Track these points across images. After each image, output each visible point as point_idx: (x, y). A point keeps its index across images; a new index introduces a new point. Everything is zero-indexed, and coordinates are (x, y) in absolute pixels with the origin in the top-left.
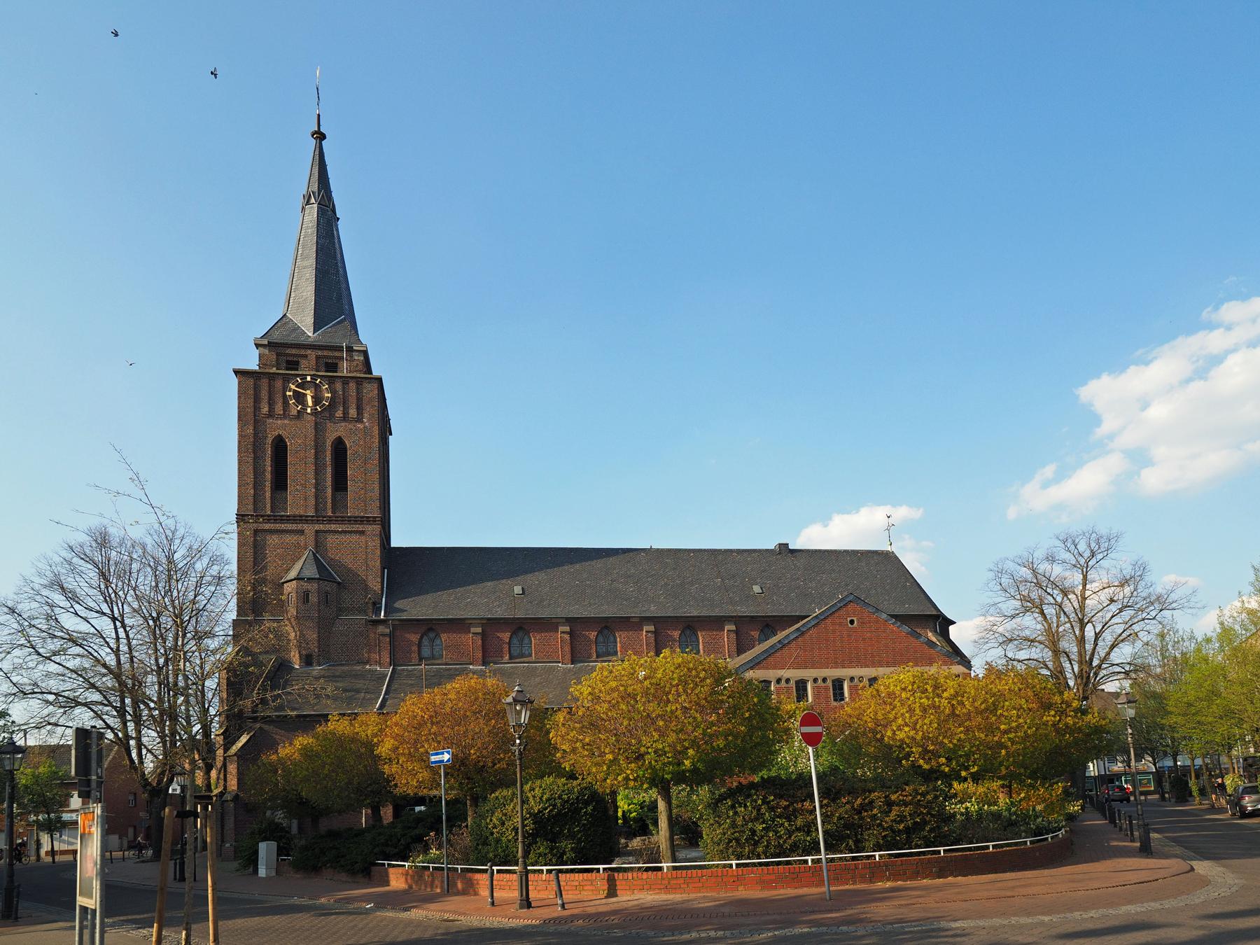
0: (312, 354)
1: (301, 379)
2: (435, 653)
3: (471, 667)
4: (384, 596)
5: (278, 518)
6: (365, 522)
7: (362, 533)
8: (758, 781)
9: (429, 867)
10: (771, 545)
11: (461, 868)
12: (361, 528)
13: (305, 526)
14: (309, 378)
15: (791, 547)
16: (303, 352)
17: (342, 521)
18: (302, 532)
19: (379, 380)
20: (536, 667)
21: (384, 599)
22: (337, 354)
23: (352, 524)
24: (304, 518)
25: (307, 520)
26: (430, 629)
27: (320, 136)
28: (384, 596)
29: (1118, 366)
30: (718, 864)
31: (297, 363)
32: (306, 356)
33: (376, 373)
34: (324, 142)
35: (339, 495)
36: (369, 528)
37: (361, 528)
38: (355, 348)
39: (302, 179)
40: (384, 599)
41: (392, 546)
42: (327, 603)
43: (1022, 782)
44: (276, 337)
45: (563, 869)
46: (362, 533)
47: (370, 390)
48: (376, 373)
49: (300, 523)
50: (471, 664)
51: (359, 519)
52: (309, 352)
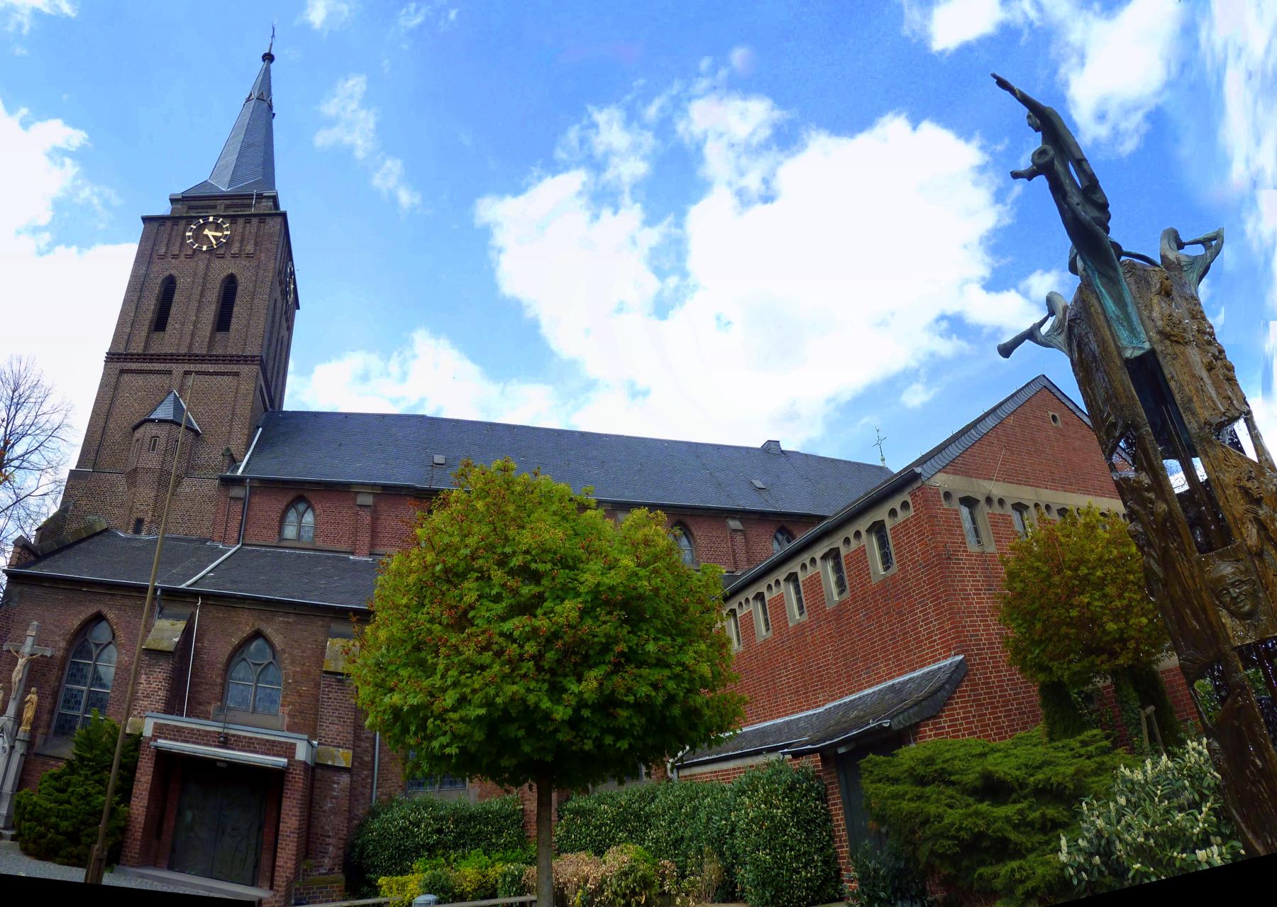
2: (302, 533)
3: (351, 557)
4: (249, 453)
7: (237, 374)
8: (499, 716)
10: (758, 443)
12: (234, 368)
13: (174, 366)
14: (211, 219)
15: (784, 447)
16: (212, 203)
17: (216, 360)
18: (169, 372)
19: (284, 215)
21: (247, 456)
22: (249, 201)
25: (177, 360)
26: (301, 499)
27: (269, 58)
28: (249, 453)
29: (1227, 163)
33: (282, 209)
34: (273, 65)
35: (219, 335)
36: (245, 369)
39: (246, 85)
40: (247, 456)
41: (285, 408)
43: (373, 692)
46: (237, 374)
47: (273, 225)
48: (282, 209)
50: (352, 553)
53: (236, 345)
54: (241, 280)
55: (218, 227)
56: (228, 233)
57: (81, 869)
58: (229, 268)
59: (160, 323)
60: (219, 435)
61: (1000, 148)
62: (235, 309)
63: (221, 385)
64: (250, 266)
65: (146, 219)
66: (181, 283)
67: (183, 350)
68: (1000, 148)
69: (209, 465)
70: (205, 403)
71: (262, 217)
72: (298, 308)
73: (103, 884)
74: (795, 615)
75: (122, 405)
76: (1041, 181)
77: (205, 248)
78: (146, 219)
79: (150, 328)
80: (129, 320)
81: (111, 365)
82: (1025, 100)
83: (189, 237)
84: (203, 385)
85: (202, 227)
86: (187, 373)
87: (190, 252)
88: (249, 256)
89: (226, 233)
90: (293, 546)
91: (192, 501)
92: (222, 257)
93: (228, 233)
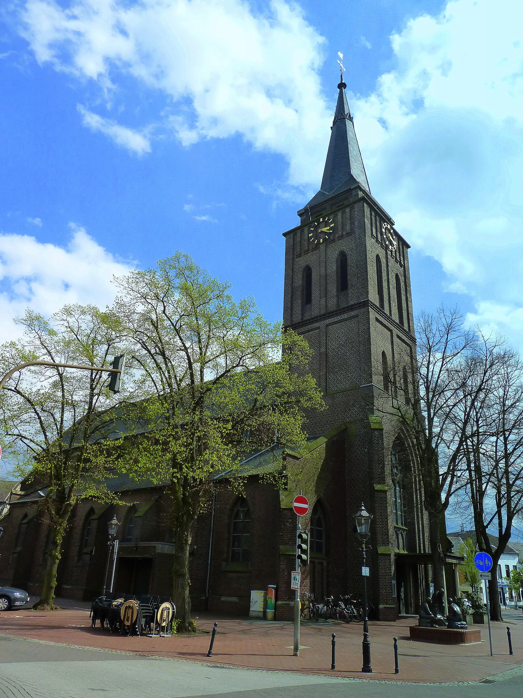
25: (307, 323)
54: (348, 253)
55: (326, 224)
56: (333, 225)
57: (473, 524)
59: (308, 299)
61: (274, 205)
65: (285, 235)
67: (323, 312)
68: (274, 205)
72: (408, 247)
73: (474, 529)
74: (480, 434)
77: (321, 241)
78: (285, 235)
79: (302, 302)
83: (311, 237)
85: (316, 228)
86: (327, 325)
87: (314, 246)
89: (331, 226)
92: (334, 241)
93: (333, 225)
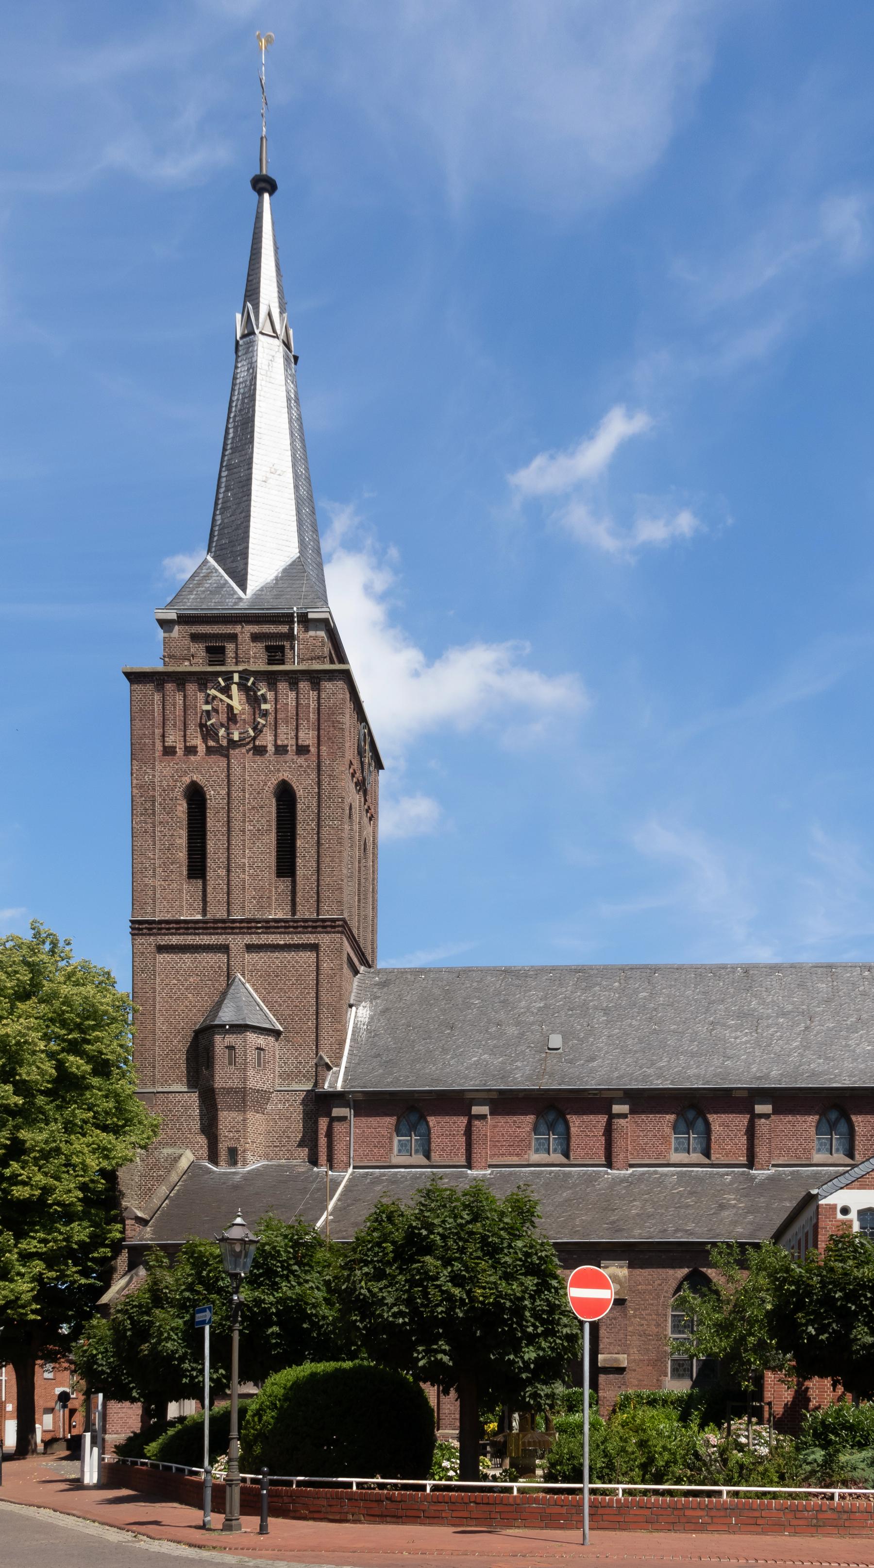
0: (245, 632)
1: (224, 680)
3: (469, 1172)
5: (318, 924)
6: (145, 931)
9: (158, 1465)
11: (163, 1466)
12: (311, 939)
20: (570, 1172)
23: (300, 933)
24: (328, 923)
25: (233, 928)
30: (676, 1483)
31: (222, 650)
32: (233, 638)
37: (311, 939)
38: (311, 616)
42: (259, 1065)
44: (191, 604)
45: (659, 1490)
46: (315, 947)
49: (221, 934)
51: (310, 924)
52: (238, 629)
53: (308, 901)
58: (279, 770)
60: (305, 1032)
62: (299, 843)
63: (297, 962)
64: (308, 766)
66: (215, 797)
69: (300, 1072)
70: (281, 989)
71: (315, 678)
72: (379, 766)
75: (171, 997)
76: (202, 1524)
80: (394, 1520)
81: (140, 940)
82: (214, 1530)
84: (274, 963)
88: (302, 750)
90: (407, 1163)
91: (288, 1119)
